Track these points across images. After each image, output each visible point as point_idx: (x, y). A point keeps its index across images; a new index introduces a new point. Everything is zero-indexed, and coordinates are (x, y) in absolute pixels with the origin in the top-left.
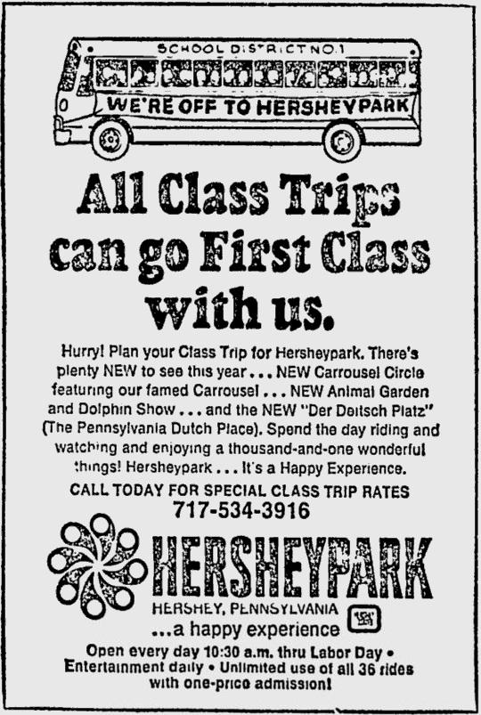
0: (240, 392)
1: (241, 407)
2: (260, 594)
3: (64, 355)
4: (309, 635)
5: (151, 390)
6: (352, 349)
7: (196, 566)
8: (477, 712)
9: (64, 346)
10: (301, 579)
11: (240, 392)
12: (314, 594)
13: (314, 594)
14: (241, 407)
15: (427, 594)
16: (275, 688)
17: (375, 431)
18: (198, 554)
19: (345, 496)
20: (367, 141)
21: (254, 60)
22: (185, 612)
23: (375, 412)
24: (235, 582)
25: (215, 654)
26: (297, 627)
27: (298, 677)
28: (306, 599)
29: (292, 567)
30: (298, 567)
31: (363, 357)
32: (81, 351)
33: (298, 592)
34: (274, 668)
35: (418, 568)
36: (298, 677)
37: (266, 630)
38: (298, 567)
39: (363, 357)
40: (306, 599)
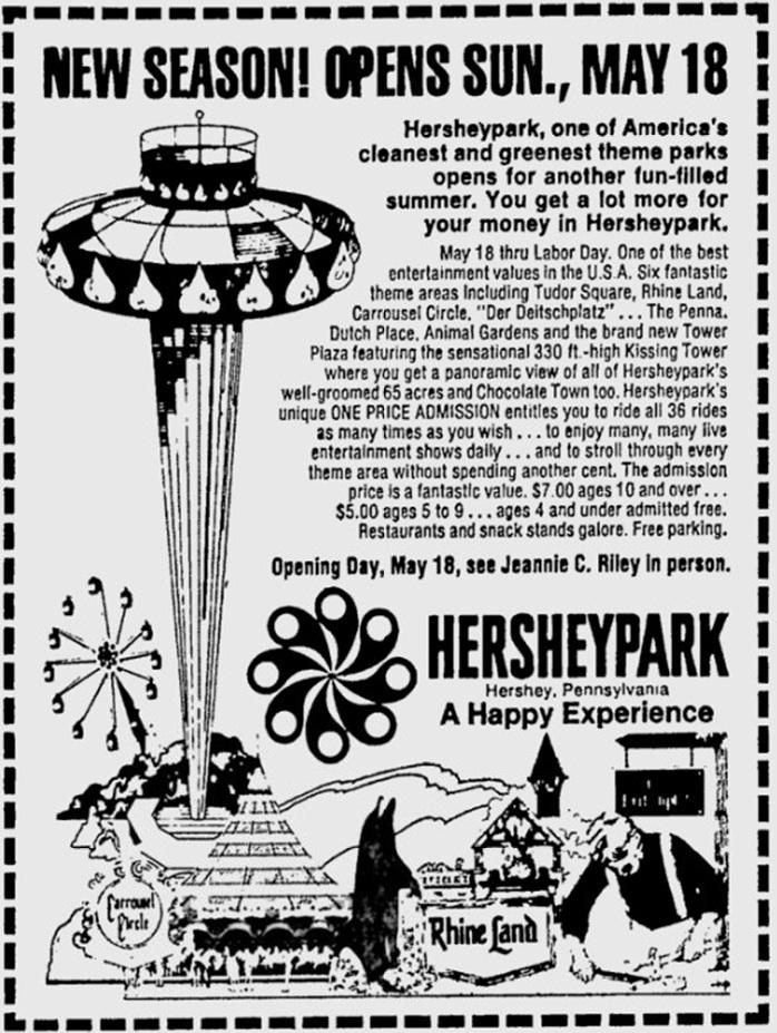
0: (401, 315)
1: (605, 146)
2: (543, 674)
3: (407, 135)
4: (370, 161)
5: (423, 492)
6: (679, 122)
7: (474, 645)
8: (49, 982)
9: (407, 123)
10: (587, 658)
11: (401, 315)
12: (601, 671)
13: (601, 671)
14: (605, 146)
15: (723, 671)
16: (413, 206)
17: (618, 412)
18: (476, 633)
19: (718, 313)
20: (146, 323)
21: (318, 479)
22: (457, 416)
23: (557, 314)
24: (515, 663)
25: (374, 514)
26: (645, 709)
27: (698, 461)
28: (591, 678)
29: (576, 645)
30: (582, 645)
31: (725, 229)
32: (410, 201)
33: (581, 672)
34: (661, 713)
35: (712, 644)
36: (698, 461)
37: (595, 715)
38: (582, 645)
39: (725, 229)
40: (591, 678)
